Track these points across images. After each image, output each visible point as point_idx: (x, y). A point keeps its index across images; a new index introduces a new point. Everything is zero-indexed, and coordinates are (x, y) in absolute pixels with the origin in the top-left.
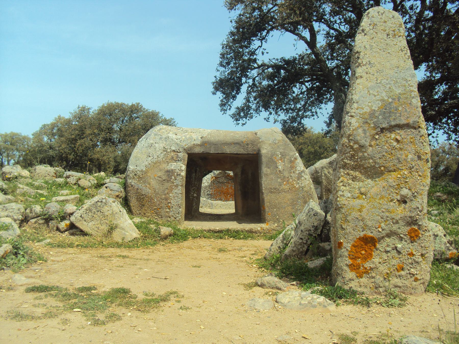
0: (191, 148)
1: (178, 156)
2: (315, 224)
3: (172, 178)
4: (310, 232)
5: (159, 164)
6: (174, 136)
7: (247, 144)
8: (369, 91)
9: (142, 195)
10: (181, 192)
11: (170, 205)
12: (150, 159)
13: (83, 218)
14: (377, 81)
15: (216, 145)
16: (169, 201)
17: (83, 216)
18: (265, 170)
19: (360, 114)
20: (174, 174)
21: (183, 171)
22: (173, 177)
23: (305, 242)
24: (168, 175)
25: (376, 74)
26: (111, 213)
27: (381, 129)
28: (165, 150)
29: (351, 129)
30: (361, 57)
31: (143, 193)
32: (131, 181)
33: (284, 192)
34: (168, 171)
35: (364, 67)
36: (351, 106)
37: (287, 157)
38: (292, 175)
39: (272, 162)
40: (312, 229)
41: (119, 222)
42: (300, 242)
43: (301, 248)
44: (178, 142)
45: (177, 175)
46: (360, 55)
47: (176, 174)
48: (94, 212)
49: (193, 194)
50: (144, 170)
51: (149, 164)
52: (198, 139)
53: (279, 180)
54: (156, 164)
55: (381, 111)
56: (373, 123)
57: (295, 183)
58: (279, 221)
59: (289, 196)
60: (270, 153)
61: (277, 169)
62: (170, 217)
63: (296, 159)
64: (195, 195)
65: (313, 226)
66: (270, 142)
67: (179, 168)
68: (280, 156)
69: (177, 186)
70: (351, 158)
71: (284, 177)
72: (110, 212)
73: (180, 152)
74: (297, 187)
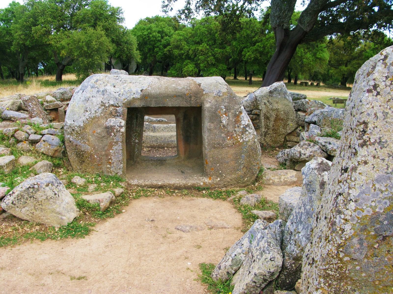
0: (130, 102)
1: (116, 112)
2: (272, 270)
3: (111, 135)
4: (265, 278)
5: (97, 120)
6: (113, 89)
7: (190, 97)
8: (374, 185)
9: (82, 151)
10: (121, 148)
11: (110, 161)
12: (87, 114)
13: (15, 204)
14: (387, 169)
15: (157, 98)
16: (109, 157)
17: (14, 202)
18: (207, 124)
19: (358, 218)
20: (113, 131)
21: (122, 127)
22: (113, 134)
23: (258, 285)
24: (107, 132)
25: (387, 159)
26: (45, 198)
27: (384, 237)
28: (103, 104)
29: (344, 239)
30: (369, 131)
31: (83, 150)
32: (69, 136)
33: (228, 147)
34: (107, 128)
35: (371, 148)
36: (346, 205)
37: (232, 111)
38: (236, 129)
39: (216, 117)
40: (267, 274)
41: (54, 207)
42: (253, 285)
43: (254, 290)
44: (116, 95)
45: (117, 131)
46: (367, 127)
47: (115, 130)
48: (27, 198)
49: (135, 140)
50: (82, 125)
51: (87, 119)
52: (137, 92)
53: (223, 135)
54: (93, 120)
55: (387, 214)
56: (374, 230)
57: (239, 137)
58: (222, 176)
59: (232, 151)
60: (214, 107)
61: (221, 124)
62: (111, 173)
63: (241, 112)
64: (137, 141)
65: (269, 272)
66: (214, 95)
67: (118, 124)
68: (224, 110)
69: (117, 143)
70: (337, 270)
71: (228, 132)
72: (44, 197)
73: (119, 106)
74: (241, 141)
